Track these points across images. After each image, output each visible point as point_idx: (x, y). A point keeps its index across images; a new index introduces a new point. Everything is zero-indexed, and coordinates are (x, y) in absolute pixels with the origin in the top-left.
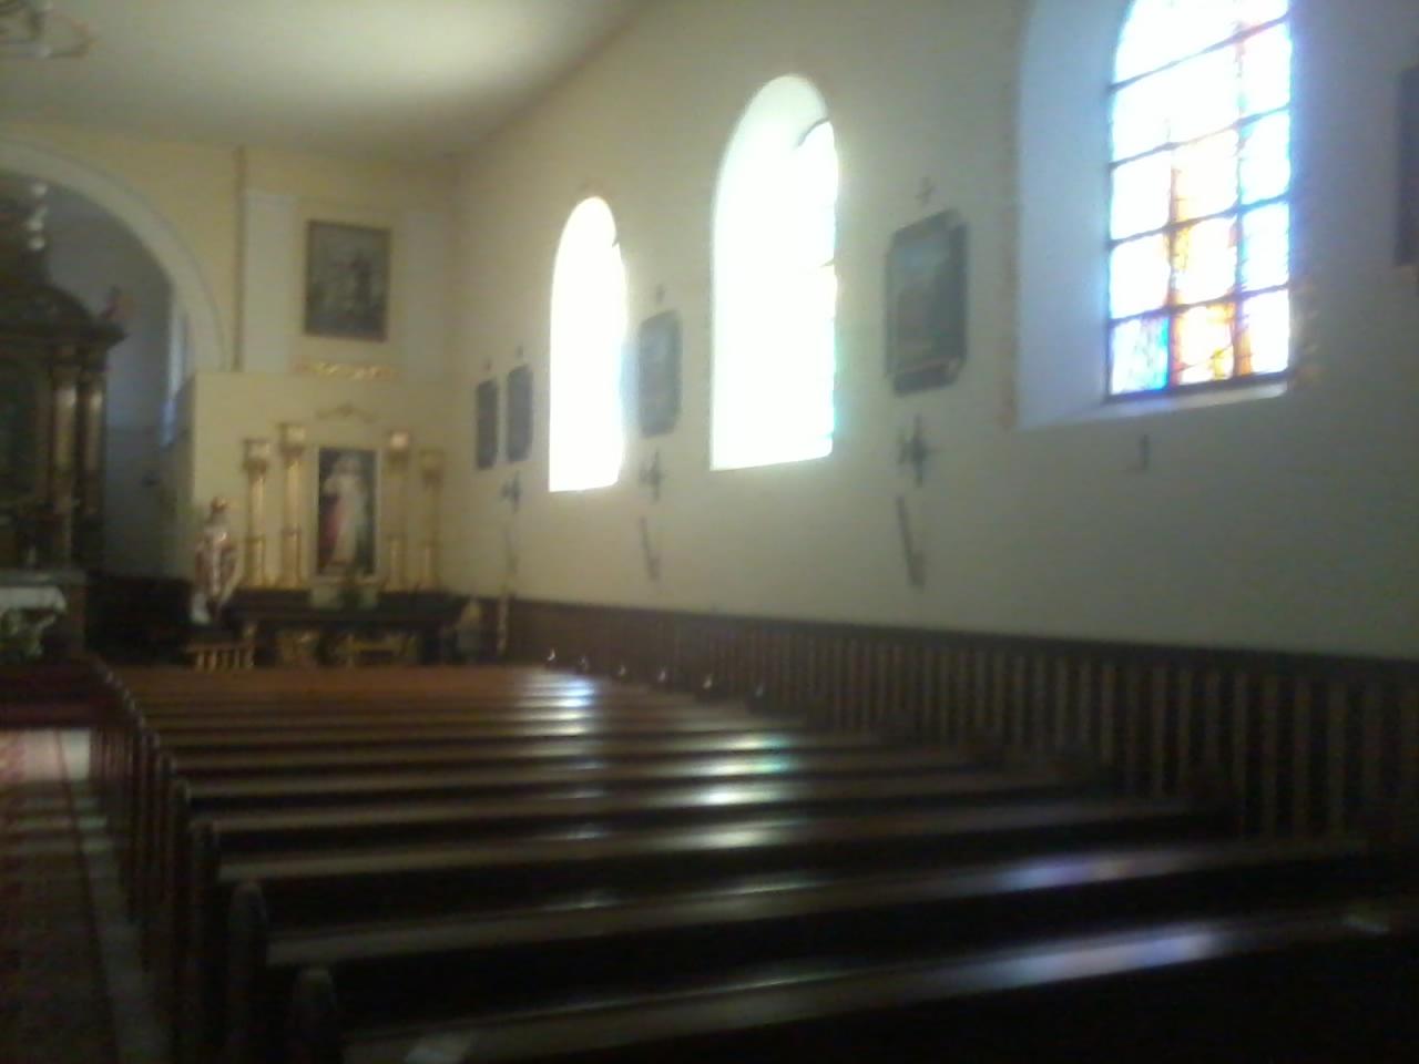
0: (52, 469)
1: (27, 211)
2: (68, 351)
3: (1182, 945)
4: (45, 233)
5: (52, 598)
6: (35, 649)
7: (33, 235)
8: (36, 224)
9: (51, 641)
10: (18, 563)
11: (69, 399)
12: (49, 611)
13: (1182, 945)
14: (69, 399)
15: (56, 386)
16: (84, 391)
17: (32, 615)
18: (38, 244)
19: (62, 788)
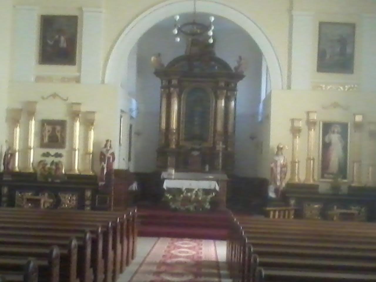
0: (215, 131)
1: (208, 28)
2: (222, 84)
3: (175, 107)
4: (213, 37)
5: (214, 185)
6: (208, 206)
7: (209, 37)
8: (211, 33)
9: (213, 203)
10: (202, 170)
11: (222, 103)
12: (215, 190)
13: (175, 107)
14: (222, 103)
15: (217, 98)
16: (228, 100)
17: (207, 192)
18: (211, 41)
19: (216, 265)
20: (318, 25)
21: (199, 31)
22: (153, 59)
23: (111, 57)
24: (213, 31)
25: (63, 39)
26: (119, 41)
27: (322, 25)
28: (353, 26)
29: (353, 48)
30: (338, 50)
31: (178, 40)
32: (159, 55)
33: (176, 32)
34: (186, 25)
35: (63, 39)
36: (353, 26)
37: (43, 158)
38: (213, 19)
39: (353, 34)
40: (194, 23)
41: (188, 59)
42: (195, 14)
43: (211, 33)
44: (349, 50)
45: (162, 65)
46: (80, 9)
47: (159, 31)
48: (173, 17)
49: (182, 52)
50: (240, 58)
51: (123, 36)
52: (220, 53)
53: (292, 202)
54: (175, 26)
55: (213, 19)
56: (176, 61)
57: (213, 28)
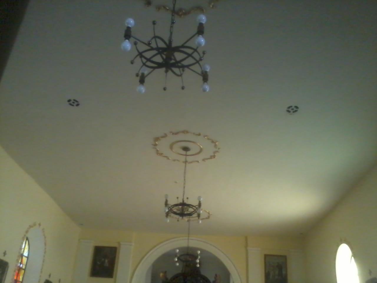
1: (196, 258)
4: (200, 264)
7: (197, 263)
8: (198, 261)
18: (198, 266)
20: (263, 257)
21: (190, 259)
22: (161, 275)
23: (138, 269)
24: (200, 260)
25: (106, 261)
26: (141, 264)
27: (266, 256)
28: (285, 257)
29: (286, 271)
30: (277, 272)
31: (178, 264)
32: (165, 272)
33: (176, 260)
34: (181, 255)
35: (106, 261)
36: (285, 257)
37: (288, 109)
38: (199, 252)
39: (285, 263)
40: (188, 254)
41: (184, 275)
42: (188, 248)
43: (198, 261)
44: (284, 272)
45: (167, 279)
46: (119, 243)
47: (167, 257)
48: (174, 250)
49: (179, 271)
50: (216, 275)
51: (143, 261)
52: (203, 273)
53: (211, 6)
54: (176, 256)
55: (199, 252)
56: (176, 277)
57: (199, 257)
